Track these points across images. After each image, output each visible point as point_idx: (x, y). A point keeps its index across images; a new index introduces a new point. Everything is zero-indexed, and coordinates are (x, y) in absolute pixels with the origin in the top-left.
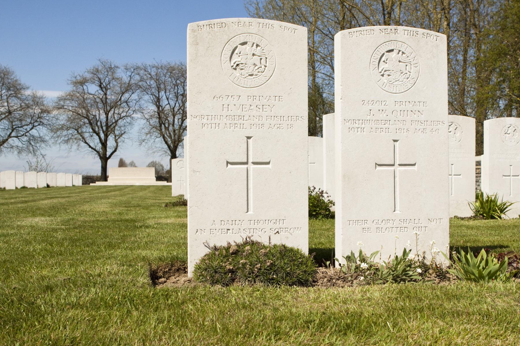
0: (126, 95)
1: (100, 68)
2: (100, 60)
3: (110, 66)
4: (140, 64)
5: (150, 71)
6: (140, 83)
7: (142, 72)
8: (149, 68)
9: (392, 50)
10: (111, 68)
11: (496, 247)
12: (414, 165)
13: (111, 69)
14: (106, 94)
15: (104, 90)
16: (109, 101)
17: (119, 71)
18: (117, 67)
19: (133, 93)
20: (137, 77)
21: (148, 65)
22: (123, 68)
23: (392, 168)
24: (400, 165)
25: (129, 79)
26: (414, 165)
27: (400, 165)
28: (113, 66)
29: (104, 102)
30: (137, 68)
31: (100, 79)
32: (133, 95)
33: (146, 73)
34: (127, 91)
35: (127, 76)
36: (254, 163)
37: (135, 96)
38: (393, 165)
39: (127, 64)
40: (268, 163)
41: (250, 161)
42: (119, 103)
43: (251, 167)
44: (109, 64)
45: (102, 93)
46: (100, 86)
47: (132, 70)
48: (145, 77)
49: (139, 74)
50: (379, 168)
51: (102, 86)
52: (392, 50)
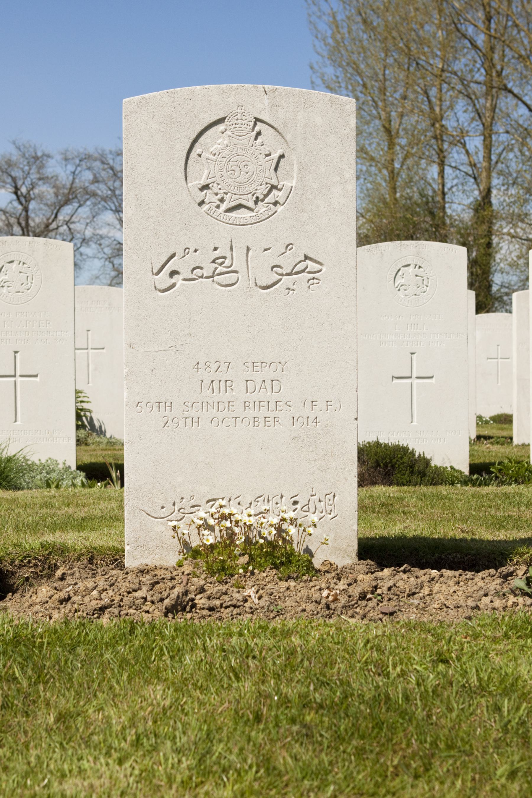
0: (67, 210)
1: (14, 158)
2: (14, 143)
3: (33, 154)
4: (91, 150)
5: (111, 162)
6: (93, 187)
7: (97, 164)
8: (110, 156)
9: (12, 262)
10: (36, 158)
11: (428, 525)
12: (432, 377)
13: (37, 160)
14: (26, 209)
15: (23, 200)
16: (32, 224)
17: (51, 163)
18: (48, 156)
19: (80, 206)
20: (88, 176)
21: (107, 152)
22: (59, 157)
23: (408, 381)
24: (417, 378)
25: (71, 178)
26: (432, 377)
27: (417, 378)
28: (39, 154)
29: (23, 223)
30: (89, 157)
31: (14, 180)
32: (80, 210)
33: (106, 166)
34: (67, 202)
35: (68, 172)
36: (21, 376)
37: (84, 211)
38: (411, 377)
39: (67, 151)
40: (36, 376)
41: (18, 374)
42: (54, 225)
43: (19, 380)
44: (31, 150)
45: (20, 207)
46: (16, 193)
47: (77, 161)
48: (103, 174)
49: (89, 169)
50: (396, 381)
51: (19, 193)
52: (12, 262)
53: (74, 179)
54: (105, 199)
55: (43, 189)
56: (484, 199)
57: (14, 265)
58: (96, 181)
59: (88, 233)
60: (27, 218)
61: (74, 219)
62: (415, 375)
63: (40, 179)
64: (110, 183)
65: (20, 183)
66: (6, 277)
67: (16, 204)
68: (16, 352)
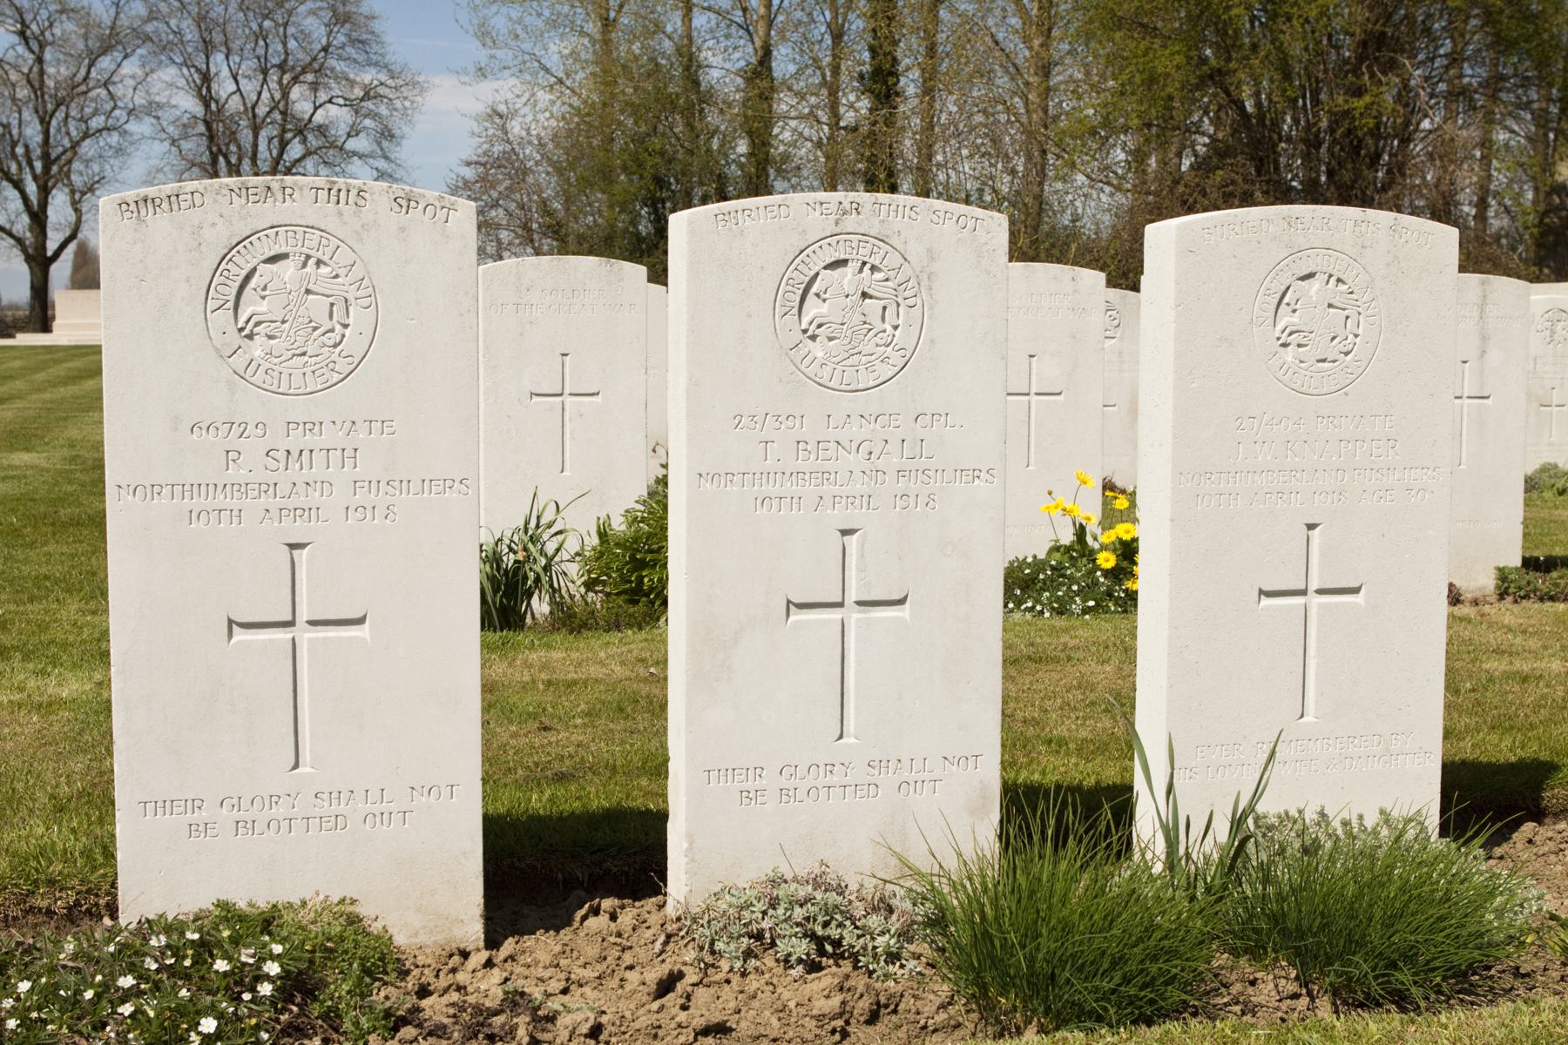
0: (105, 63)
6: (149, 28)
9: (1311, 276)
14: (40, 60)
29: (37, 85)
34: (105, 51)
36: (1320, 592)
37: (131, 68)
40: (1356, 591)
46: (22, 34)
51: (28, 33)
52: (1311, 276)
53: (117, 13)
54: (164, 48)
55: (66, 27)
56: (761, 63)
57: (1315, 285)
58: (151, 17)
59: (140, 100)
60: (42, 73)
61: (115, 79)
62: (1034, 390)
63: (62, 12)
64: (173, 23)
65: (28, 17)
66: (1295, 319)
67: (21, 49)
68: (1311, 527)
